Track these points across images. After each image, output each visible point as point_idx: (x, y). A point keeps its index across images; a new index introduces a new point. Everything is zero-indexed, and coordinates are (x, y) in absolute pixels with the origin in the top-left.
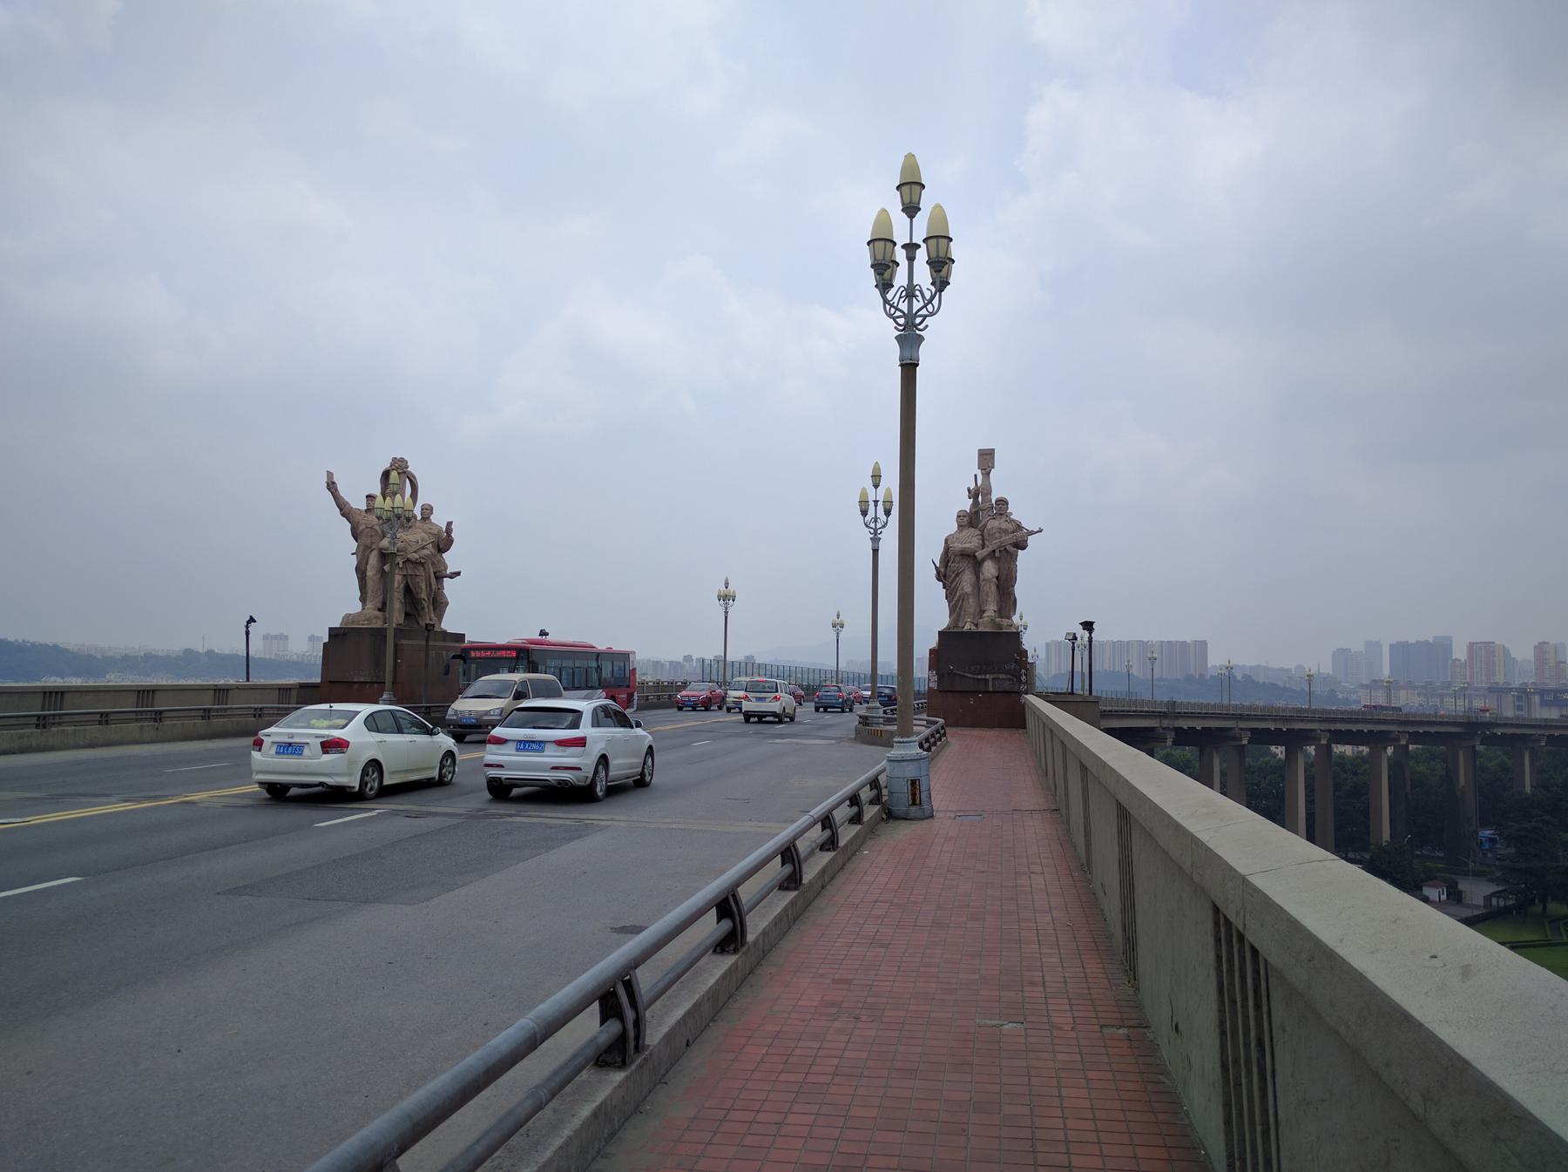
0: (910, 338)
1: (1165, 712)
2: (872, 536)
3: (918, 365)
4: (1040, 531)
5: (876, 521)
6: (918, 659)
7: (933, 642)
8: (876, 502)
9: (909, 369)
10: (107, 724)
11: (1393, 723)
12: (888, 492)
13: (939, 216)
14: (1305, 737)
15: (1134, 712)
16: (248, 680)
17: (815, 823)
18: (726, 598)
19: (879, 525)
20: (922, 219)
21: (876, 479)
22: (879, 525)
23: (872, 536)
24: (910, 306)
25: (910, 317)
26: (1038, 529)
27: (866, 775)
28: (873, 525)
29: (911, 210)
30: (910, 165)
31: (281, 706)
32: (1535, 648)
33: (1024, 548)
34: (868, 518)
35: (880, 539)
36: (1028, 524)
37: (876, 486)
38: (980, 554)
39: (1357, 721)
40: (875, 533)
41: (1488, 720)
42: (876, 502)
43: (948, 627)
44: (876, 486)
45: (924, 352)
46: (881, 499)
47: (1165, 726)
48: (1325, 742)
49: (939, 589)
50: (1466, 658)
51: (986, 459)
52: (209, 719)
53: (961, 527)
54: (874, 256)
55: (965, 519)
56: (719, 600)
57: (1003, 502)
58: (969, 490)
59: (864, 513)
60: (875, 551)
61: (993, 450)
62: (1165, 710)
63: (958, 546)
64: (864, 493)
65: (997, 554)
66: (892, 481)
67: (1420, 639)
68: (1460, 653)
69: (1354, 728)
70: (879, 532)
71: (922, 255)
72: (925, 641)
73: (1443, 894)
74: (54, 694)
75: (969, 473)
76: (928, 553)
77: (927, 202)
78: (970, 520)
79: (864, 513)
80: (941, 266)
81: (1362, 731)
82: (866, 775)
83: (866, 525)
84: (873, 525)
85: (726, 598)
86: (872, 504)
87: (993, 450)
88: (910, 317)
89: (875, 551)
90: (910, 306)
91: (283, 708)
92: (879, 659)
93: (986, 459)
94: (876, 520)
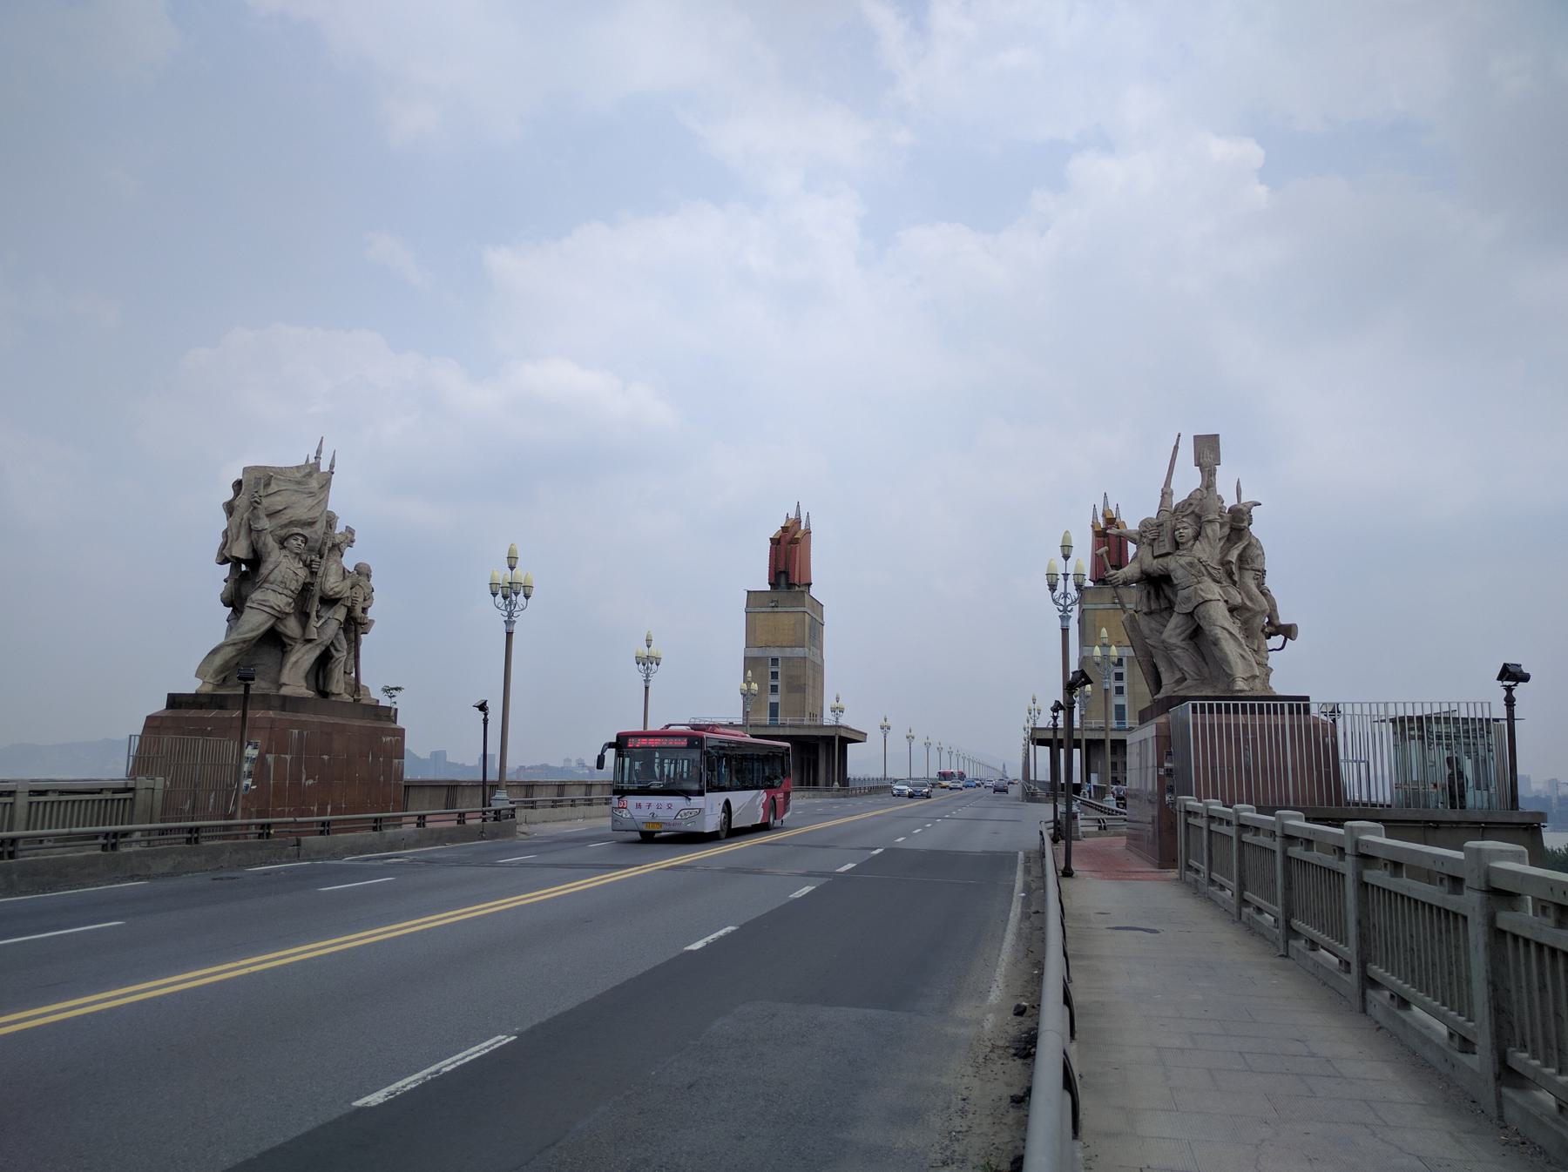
2: (1061, 613)
5: (1065, 597)
8: (1066, 575)
10: (328, 834)
16: (1468, 888)
18: (647, 662)
19: (1069, 602)
22: (1069, 602)
23: (1061, 613)
24: (1065, 601)
27: (1235, 860)
28: (1062, 601)
30: (1066, 537)
31: (448, 811)
34: (1057, 593)
35: (515, 622)
37: (1066, 557)
40: (1065, 610)
42: (1066, 575)
44: (1066, 557)
46: (1071, 571)
52: (381, 830)
56: (638, 664)
59: (1053, 587)
60: (509, 635)
67: (221, 592)
70: (1069, 608)
74: (116, 801)
82: (1235, 860)
83: (1054, 600)
84: (1062, 601)
85: (647, 662)
86: (1061, 577)
89: (509, 635)
90: (1065, 601)
91: (345, 820)
92: (488, 752)
94: (1065, 596)
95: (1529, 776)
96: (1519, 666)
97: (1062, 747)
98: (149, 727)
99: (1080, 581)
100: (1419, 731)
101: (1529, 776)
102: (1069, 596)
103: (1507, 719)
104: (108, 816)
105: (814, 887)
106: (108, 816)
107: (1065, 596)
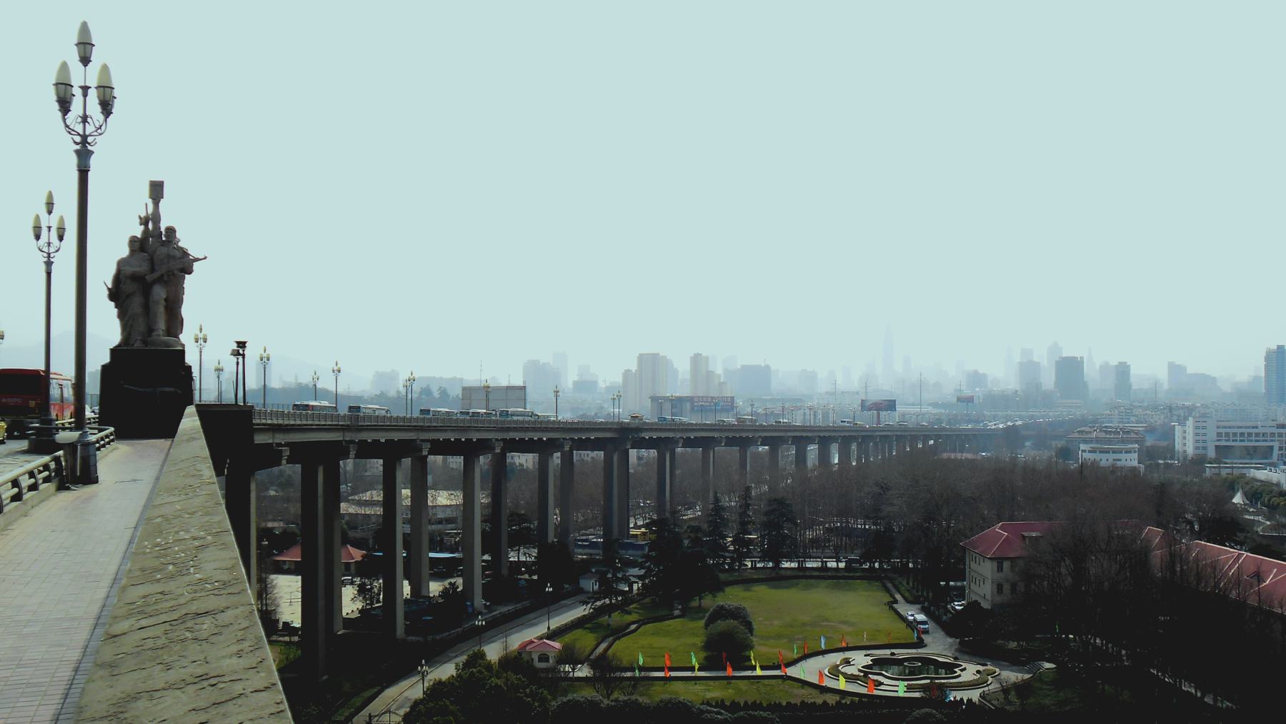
0: (84, 155)
1: (348, 425)
3: (89, 170)
4: (205, 258)
6: (91, 373)
7: (106, 359)
8: (85, 89)
9: (49, 274)
11: (558, 431)
12: (62, 220)
13: (105, 69)
14: (483, 446)
15: (317, 425)
17: (24, 474)
20: (94, 67)
21: (50, 207)
22: (52, 250)
23: (78, 147)
25: (84, 138)
26: (203, 257)
28: (46, 249)
29: (85, 60)
32: (691, 358)
33: (190, 273)
34: (71, 117)
35: (53, 262)
36: (193, 252)
38: (149, 278)
39: (526, 430)
41: (637, 425)
42: (85, 89)
43: (119, 345)
44: (50, 212)
45: (93, 161)
46: (93, 82)
47: (348, 439)
48: (499, 451)
49: (111, 309)
50: (636, 368)
51: (157, 190)
53: (132, 251)
54: (58, 94)
55: (137, 244)
57: (171, 231)
58: (140, 218)
59: (65, 105)
61: (163, 182)
62: (349, 423)
63: (129, 270)
64: (64, 67)
65: (165, 278)
66: (67, 209)
68: (541, 364)
69: (527, 436)
71: (93, 95)
72: (98, 358)
73: (596, 584)
75: (143, 205)
76: (101, 275)
77: (97, 57)
78: (138, 245)
79: (38, 237)
80: (107, 107)
81: (524, 439)
84: (46, 249)
86: (77, 92)
87: (163, 182)
88: (84, 138)
92: (246, 389)
93: (157, 190)
95: (1082, 358)
96: (59, 110)
97: (406, 601)
98: (487, 393)
99: (107, 98)
100: (857, 572)
101: (1082, 358)
102: (89, 120)
103: (847, 647)
104: (321, 592)
105: (1027, 676)
106: (321, 592)
107: (85, 119)
